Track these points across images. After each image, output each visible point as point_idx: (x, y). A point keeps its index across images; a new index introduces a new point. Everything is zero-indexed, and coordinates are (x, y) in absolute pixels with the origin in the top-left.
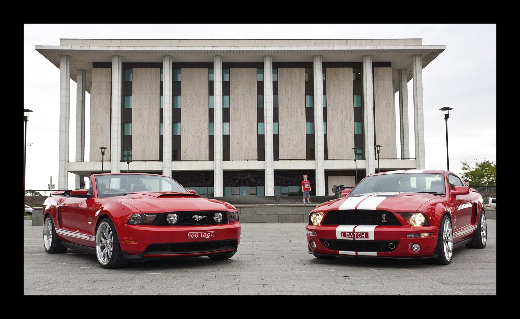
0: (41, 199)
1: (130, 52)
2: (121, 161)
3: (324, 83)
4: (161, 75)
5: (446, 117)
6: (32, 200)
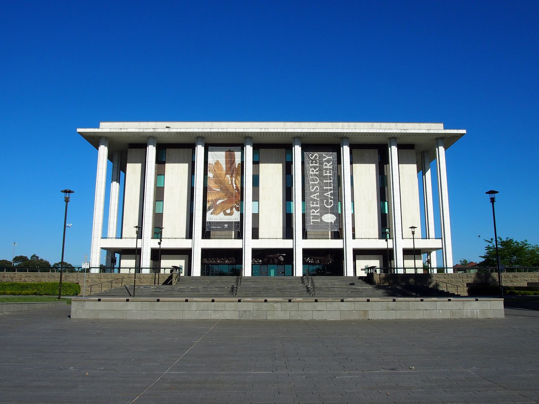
0: (74, 276)
1: (183, 134)
2: (152, 238)
3: (303, 163)
4: (193, 155)
5: (493, 200)
6: (66, 277)
